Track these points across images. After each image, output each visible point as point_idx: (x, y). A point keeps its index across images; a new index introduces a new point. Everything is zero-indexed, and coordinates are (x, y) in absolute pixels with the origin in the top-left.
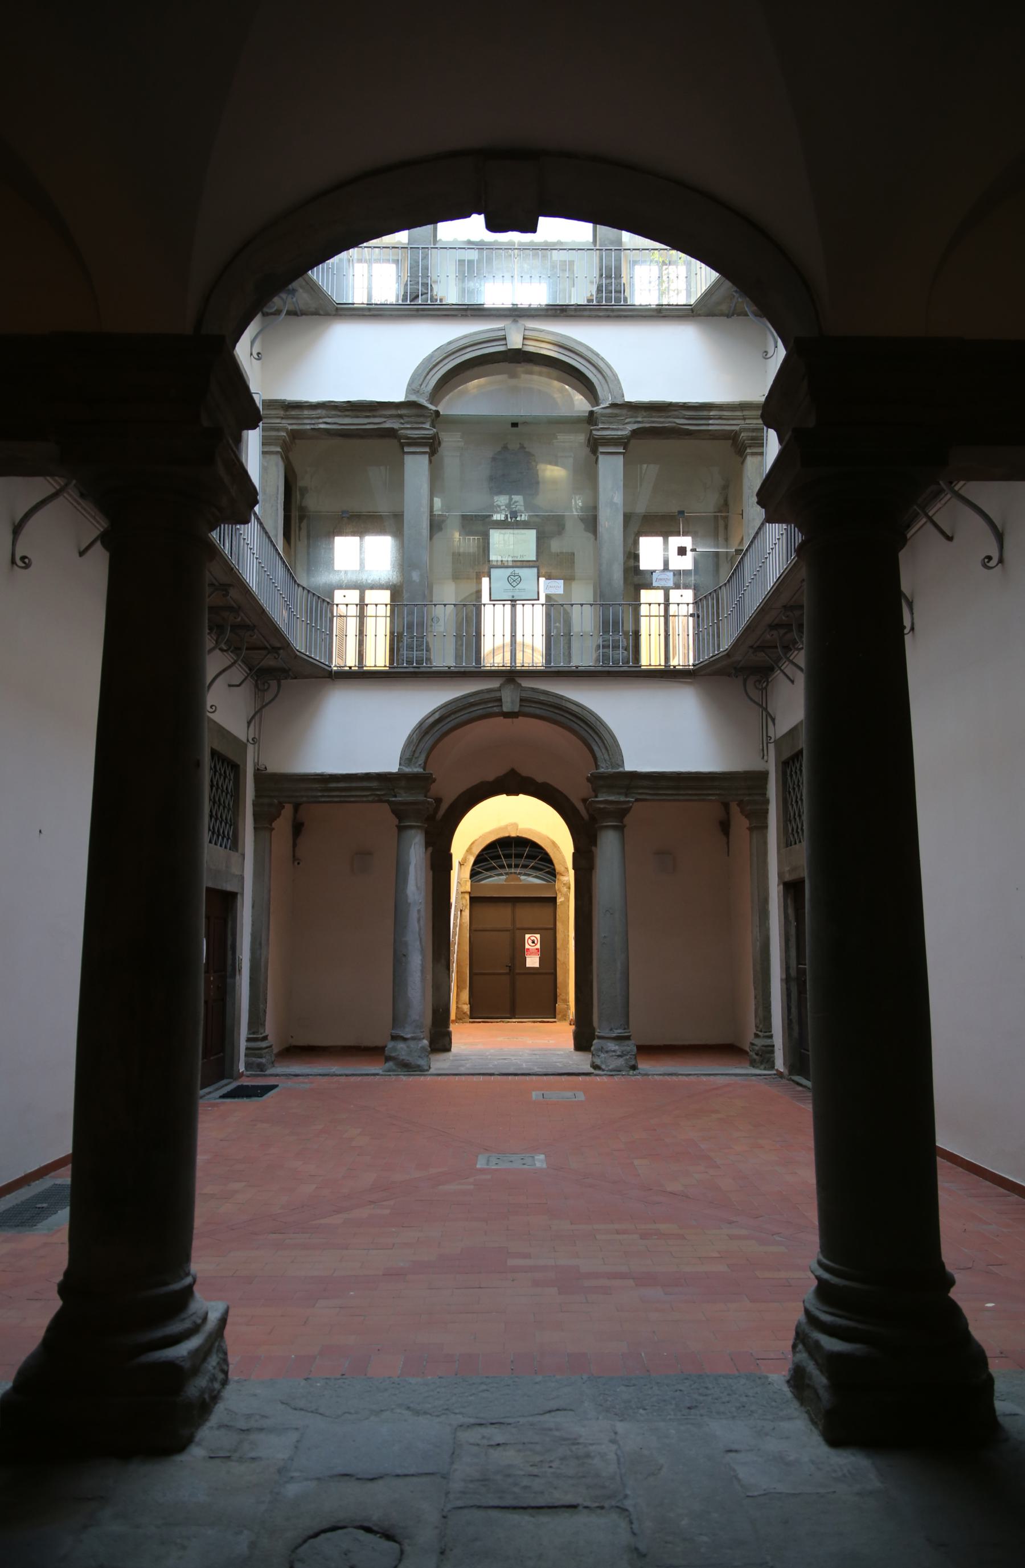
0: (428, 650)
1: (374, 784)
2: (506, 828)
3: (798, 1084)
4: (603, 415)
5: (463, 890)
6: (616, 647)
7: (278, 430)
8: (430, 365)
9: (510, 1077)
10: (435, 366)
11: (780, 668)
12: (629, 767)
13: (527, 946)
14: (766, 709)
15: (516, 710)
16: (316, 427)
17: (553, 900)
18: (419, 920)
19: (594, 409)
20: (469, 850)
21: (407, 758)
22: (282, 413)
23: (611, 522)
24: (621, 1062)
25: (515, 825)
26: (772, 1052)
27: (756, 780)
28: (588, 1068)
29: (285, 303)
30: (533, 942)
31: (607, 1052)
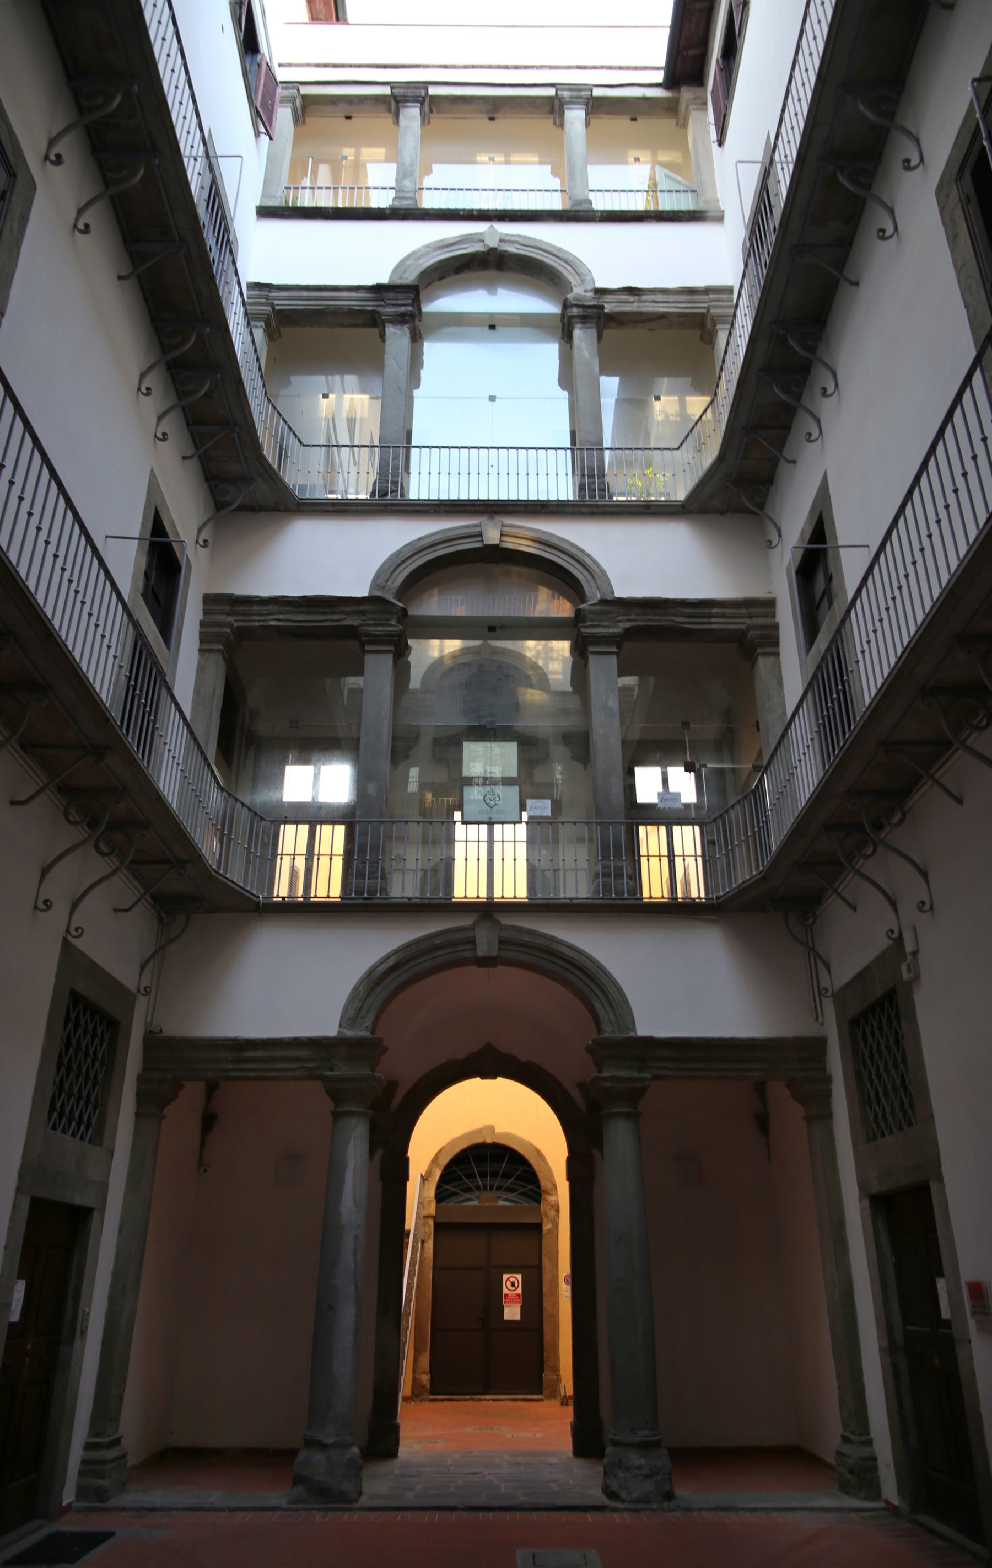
0: (384, 878)
1: (303, 1053)
2: (479, 1132)
3: (931, 1531)
4: (591, 612)
5: (426, 1212)
6: (619, 876)
8: (397, 561)
9: (481, 1515)
10: (403, 562)
11: (932, 777)
12: (642, 1030)
13: (505, 1291)
14: (813, 949)
15: (494, 953)
16: (266, 624)
17: (539, 1226)
18: (355, 1254)
19: (582, 606)
20: (435, 1161)
21: (351, 1017)
22: (227, 608)
23: (607, 734)
24: (648, 1486)
25: (492, 1128)
26: (875, 1469)
27: (810, 1050)
28: (596, 1495)
30: (513, 1285)
31: (628, 1469)
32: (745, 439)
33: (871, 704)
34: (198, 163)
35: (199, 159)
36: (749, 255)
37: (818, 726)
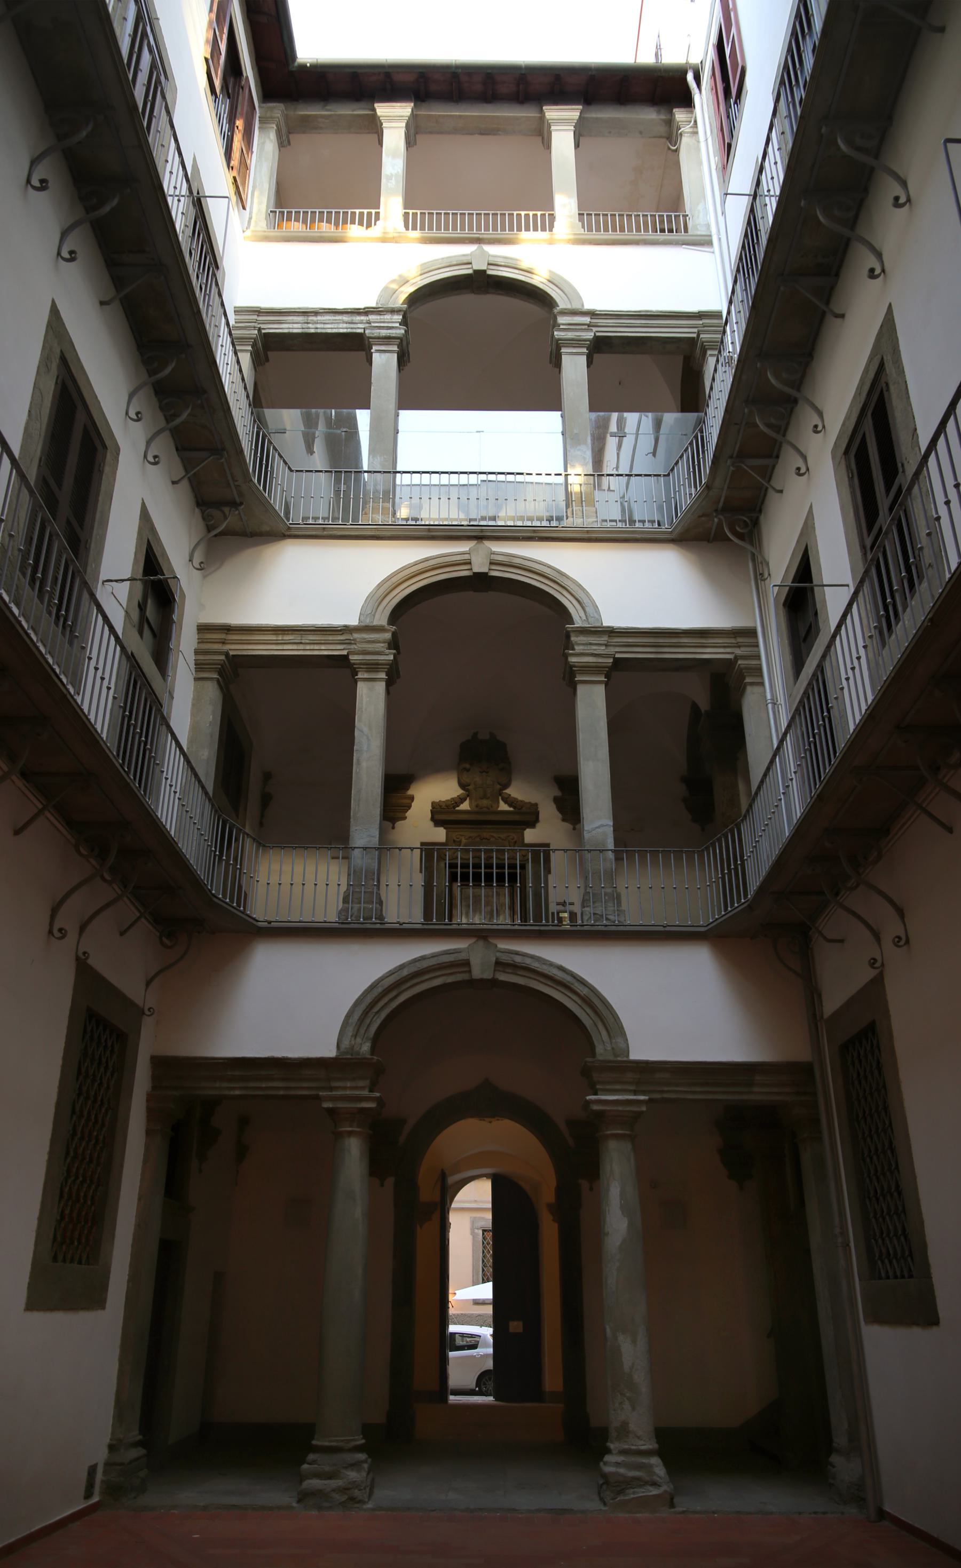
29: (226, 518)
32: (732, 468)
33: (950, 579)
34: (181, 204)
35: (182, 199)
36: (738, 270)
37: (805, 751)
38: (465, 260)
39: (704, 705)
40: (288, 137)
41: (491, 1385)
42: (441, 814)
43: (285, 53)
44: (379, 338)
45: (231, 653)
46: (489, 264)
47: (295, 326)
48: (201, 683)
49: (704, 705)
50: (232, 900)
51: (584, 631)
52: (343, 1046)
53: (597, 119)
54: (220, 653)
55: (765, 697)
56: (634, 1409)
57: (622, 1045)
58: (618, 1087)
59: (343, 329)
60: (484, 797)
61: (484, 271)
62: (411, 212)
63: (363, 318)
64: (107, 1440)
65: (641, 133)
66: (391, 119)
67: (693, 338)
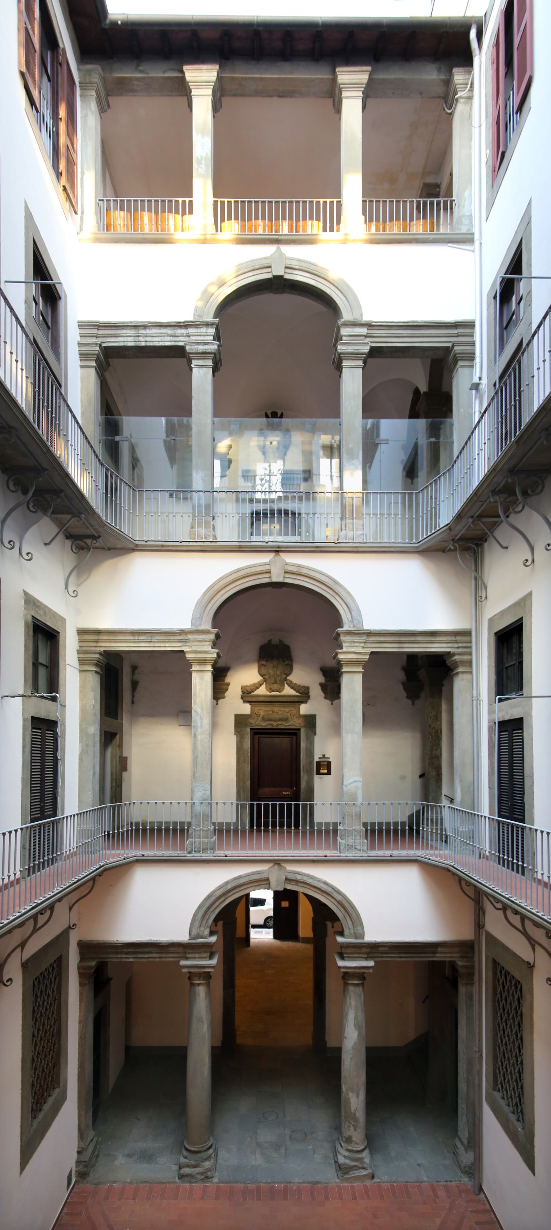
7: (91, 653)
38: (266, 263)
39: (423, 388)
40: (107, 100)
41: (271, 923)
42: (247, 695)
43: (97, 8)
44: (197, 353)
45: (104, 345)
46: (286, 268)
47: (129, 339)
48: (84, 674)
49: (423, 388)
50: (116, 524)
51: (349, 633)
52: (193, 934)
53: (384, 79)
54: (95, 653)
55: (472, 694)
56: (355, 1130)
57: (360, 931)
58: (356, 955)
59: (167, 342)
60: (275, 682)
61: (282, 276)
62: (219, 200)
63: (183, 331)
64: (76, 1149)
65: (421, 93)
66: (201, 84)
67: (448, 347)
